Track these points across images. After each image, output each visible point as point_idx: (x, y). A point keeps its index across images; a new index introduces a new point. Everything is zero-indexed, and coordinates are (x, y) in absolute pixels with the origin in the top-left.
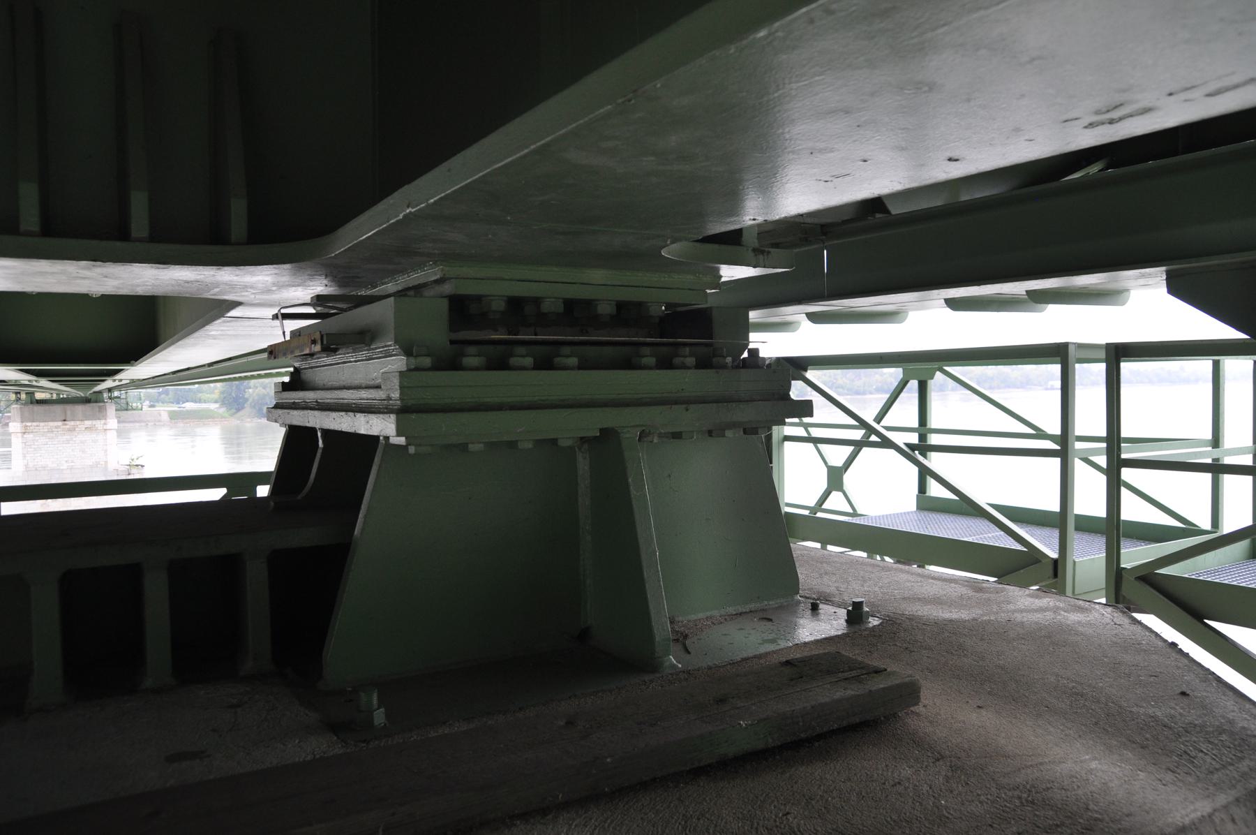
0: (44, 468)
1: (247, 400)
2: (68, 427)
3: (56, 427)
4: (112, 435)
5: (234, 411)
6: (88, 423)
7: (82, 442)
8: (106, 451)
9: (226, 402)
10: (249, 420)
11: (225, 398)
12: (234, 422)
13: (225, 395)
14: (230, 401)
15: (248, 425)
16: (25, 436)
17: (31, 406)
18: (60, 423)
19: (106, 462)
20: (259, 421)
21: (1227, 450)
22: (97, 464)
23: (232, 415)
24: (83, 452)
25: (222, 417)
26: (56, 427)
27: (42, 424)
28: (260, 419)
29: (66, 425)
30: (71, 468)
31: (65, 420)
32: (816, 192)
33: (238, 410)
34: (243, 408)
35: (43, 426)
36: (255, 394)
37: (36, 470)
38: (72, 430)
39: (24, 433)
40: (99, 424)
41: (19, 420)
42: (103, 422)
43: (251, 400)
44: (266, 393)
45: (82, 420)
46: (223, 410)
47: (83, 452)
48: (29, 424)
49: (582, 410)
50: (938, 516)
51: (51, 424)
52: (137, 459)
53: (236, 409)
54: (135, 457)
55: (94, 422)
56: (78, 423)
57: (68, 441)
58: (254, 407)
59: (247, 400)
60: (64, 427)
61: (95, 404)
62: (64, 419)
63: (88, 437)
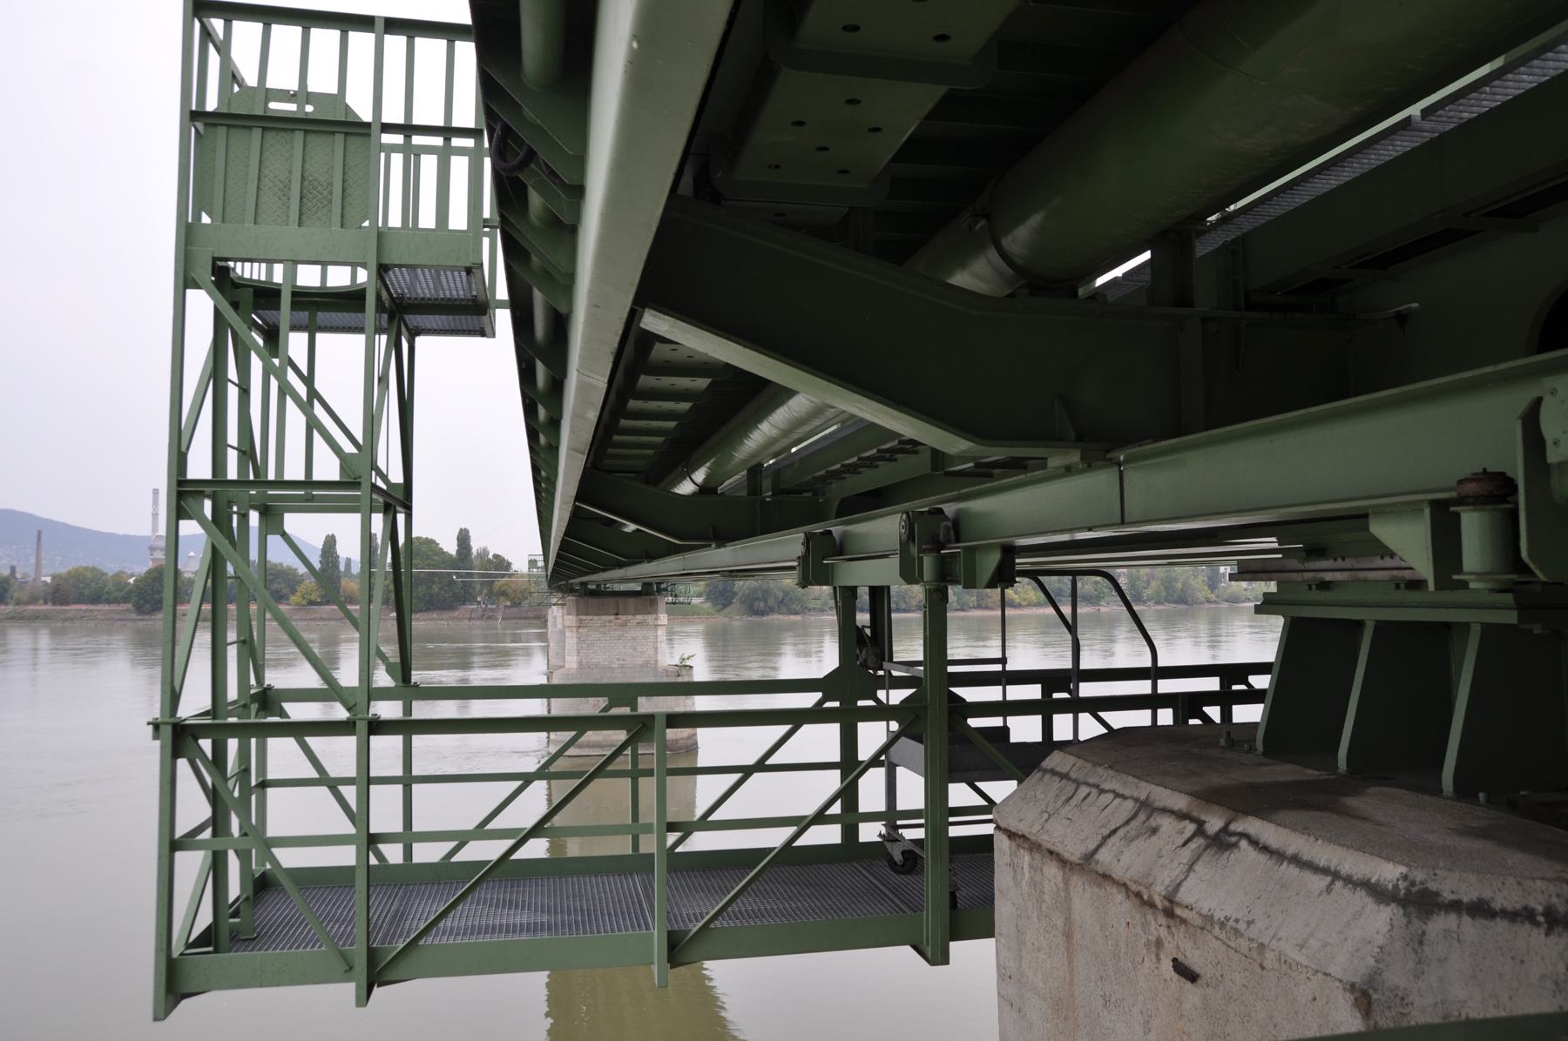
0: (596, 665)
1: (735, 594)
2: (620, 621)
3: (610, 621)
4: (661, 632)
5: (720, 606)
6: (639, 617)
7: (633, 639)
8: (656, 649)
9: (712, 596)
10: (738, 617)
11: (710, 591)
12: (720, 619)
13: (711, 588)
14: (717, 594)
15: (736, 623)
16: (580, 630)
17: (586, 598)
18: (612, 617)
19: (656, 661)
20: (750, 619)
21: (416, 833)
22: (645, 665)
23: (718, 611)
24: (634, 649)
25: (709, 614)
26: (610, 621)
27: (596, 618)
28: (751, 616)
29: (618, 619)
30: (622, 667)
31: (617, 614)
32: (214, 151)
33: (725, 606)
34: (730, 603)
35: (598, 620)
36: (745, 588)
37: (589, 667)
38: (624, 625)
39: (579, 627)
40: (650, 618)
41: (574, 612)
42: (654, 616)
43: (741, 593)
44: (757, 585)
45: (633, 615)
46: (708, 605)
47: (634, 649)
48: (583, 617)
49: (1485, 610)
50: (909, 877)
51: (604, 618)
52: (688, 659)
53: (723, 604)
54: (686, 656)
55: (646, 617)
56: (630, 617)
57: (619, 637)
58: (744, 602)
59: (735, 594)
60: (617, 621)
61: (646, 597)
62: (615, 612)
63: (639, 633)
